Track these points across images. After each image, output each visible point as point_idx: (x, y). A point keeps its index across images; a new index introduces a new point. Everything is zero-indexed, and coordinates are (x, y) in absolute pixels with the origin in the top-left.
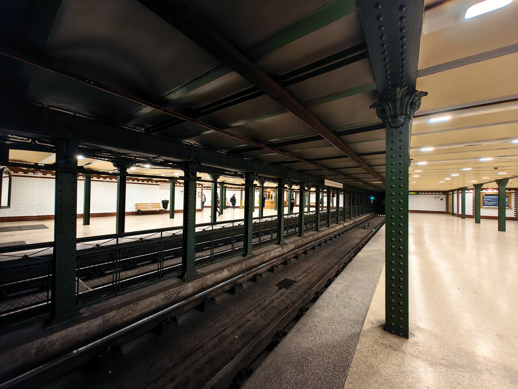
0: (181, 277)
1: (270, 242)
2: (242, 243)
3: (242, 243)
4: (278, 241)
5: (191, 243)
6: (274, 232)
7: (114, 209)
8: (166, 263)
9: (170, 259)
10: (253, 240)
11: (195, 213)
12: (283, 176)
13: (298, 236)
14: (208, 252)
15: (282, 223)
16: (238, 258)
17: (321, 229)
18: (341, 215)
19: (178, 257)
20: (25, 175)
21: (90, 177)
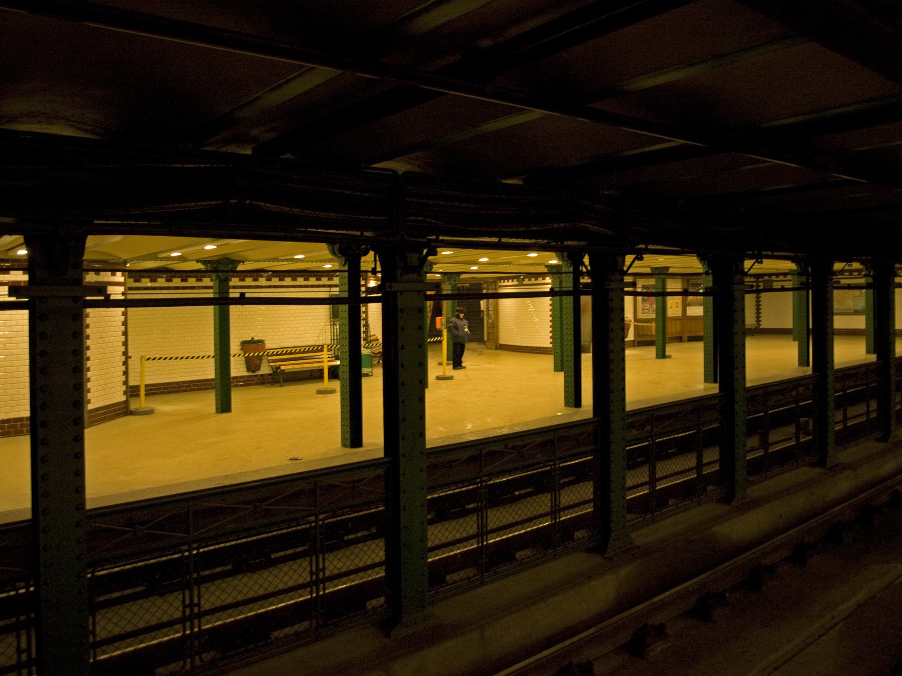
0: (388, 623)
1: (786, 458)
2: (586, 490)
3: (586, 490)
4: (815, 452)
5: (834, 391)
6: (708, 444)
7: (764, 325)
8: (212, 595)
9: (222, 576)
10: (438, 534)
11: (623, 350)
12: (594, 231)
13: (878, 440)
14: (296, 572)
15: (740, 407)
16: (803, 473)
17: (846, 455)
18: (750, 433)
19: (584, 481)
20: (137, 285)
21: (227, 280)
